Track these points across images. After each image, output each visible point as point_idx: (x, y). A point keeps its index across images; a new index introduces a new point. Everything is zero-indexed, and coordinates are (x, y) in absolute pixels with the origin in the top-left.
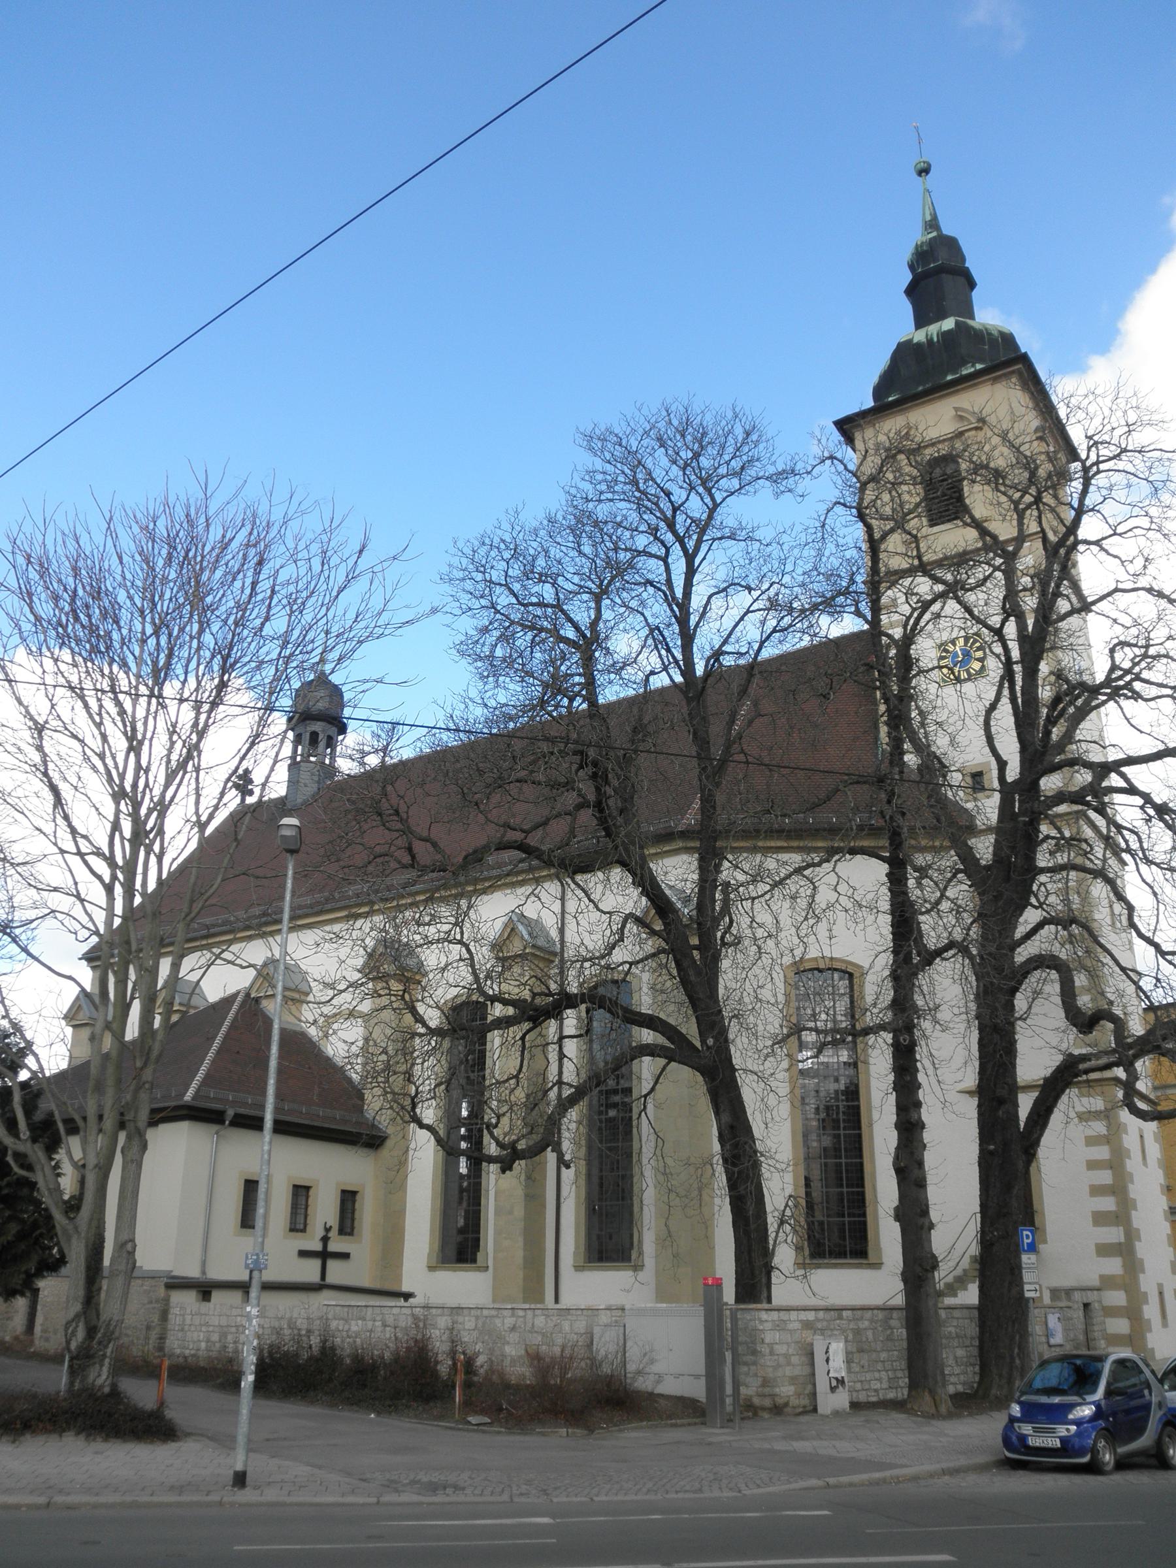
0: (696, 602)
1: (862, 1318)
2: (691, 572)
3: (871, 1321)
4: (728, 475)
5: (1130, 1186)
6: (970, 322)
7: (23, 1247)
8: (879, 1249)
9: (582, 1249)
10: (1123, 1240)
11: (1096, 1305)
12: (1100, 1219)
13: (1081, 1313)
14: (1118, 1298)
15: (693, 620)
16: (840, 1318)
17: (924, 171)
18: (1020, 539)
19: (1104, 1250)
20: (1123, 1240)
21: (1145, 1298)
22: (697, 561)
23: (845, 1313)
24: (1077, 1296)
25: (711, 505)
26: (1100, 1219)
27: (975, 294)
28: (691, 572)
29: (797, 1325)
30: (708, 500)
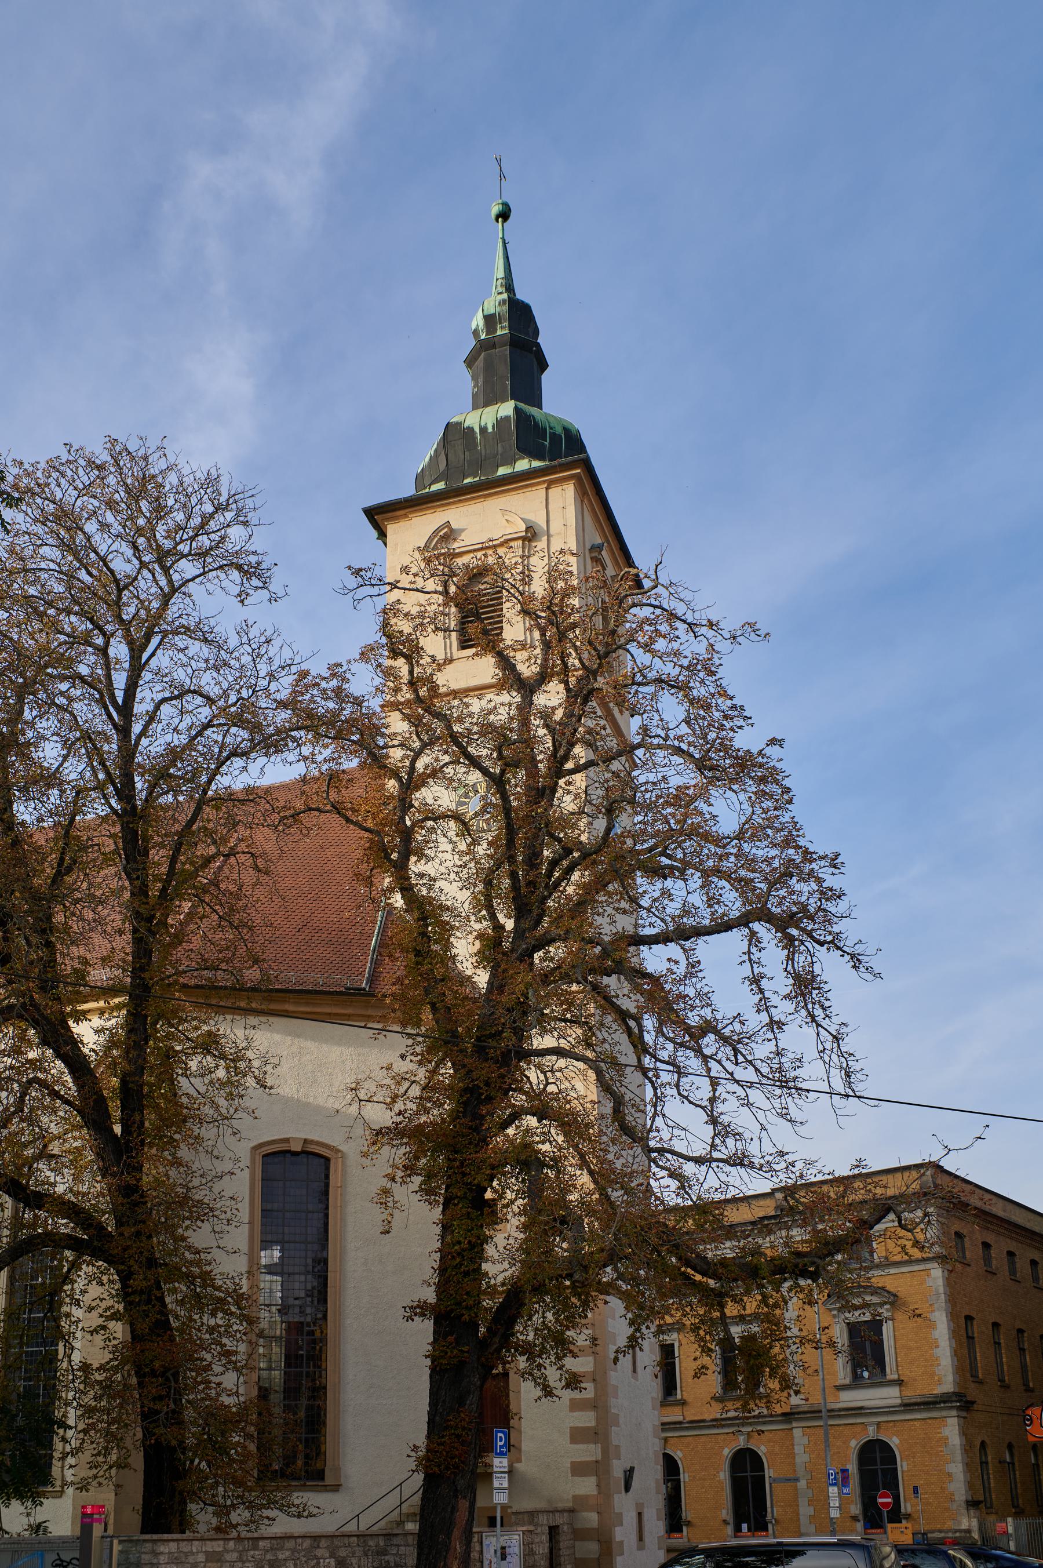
0: (140, 708)
1: (282, 1548)
2: (136, 669)
3: (293, 1551)
4: (190, 554)
5: (613, 1401)
6: (533, 411)
7: (674, 1259)
8: (337, 1470)
9: (330, 1416)
10: (599, 1458)
11: (565, 1528)
12: (578, 1435)
13: (545, 1538)
14: (591, 1519)
15: (137, 728)
16: (255, 1548)
17: (504, 215)
18: (543, 678)
19: (579, 1469)
20: (599, 1458)
21: (619, 1520)
22: (145, 656)
23: (261, 1544)
24: (543, 1519)
25: (166, 590)
26: (578, 1435)
27: (545, 377)
28: (136, 669)
29: (201, 1558)
30: (163, 582)
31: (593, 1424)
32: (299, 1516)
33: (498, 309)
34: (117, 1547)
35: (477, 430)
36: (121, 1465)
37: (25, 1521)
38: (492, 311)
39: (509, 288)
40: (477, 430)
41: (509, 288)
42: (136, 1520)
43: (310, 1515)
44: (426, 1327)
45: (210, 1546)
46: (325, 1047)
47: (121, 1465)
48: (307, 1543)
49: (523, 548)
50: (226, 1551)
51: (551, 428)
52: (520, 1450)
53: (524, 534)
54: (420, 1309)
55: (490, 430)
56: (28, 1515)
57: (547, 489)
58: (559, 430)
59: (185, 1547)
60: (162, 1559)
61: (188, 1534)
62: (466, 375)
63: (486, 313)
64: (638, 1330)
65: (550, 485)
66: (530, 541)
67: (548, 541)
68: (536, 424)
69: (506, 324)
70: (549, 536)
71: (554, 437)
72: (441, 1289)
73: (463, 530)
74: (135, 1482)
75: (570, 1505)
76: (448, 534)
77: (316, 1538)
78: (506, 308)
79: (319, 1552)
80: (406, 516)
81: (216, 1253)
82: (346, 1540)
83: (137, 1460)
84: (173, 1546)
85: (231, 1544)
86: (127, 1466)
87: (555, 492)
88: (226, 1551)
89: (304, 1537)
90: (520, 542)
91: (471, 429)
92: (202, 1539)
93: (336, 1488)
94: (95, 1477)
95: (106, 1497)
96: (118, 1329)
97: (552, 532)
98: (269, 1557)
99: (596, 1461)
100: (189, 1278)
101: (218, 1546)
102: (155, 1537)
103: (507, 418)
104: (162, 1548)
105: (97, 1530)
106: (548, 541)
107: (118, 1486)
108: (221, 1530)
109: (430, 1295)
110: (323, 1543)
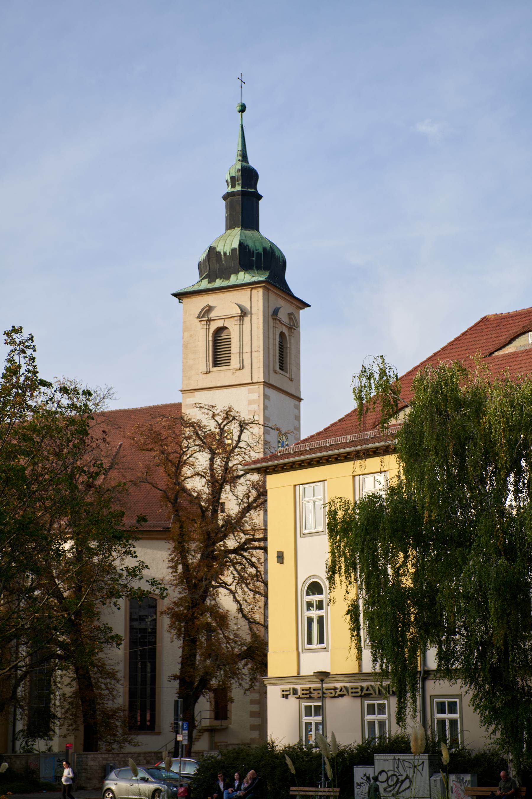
16: (118, 757)
23: (120, 755)
29: (101, 759)
31: (258, 710)
32: (135, 746)
33: (237, 174)
34: (76, 756)
35: (222, 253)
36: (76, 729)
37: (46, 747)
38: (234, 175)
39: (244, 157)
40: (222, 253)
41: (244, 157)
42: (82, 747)
43: (139, 746)
44: (177, 683)
45: (104, 756)
46: (155, 552)
47: (76, 729)
48: (136, 755)
49: (240, 320)
50: (109, 757)
51: (257, 250)
52: (231, 719)
53: (240, 315)
54: (175, 677)
55: (228, 254)
56: (47, 745)
57: (251, 290)
58: (261, 250)
59: (96, 756)
60: (89, 760)
61: (99, 752)
62: (224, 203)
63: (231, 175)
64: (253, 682)
65: (252, 289)
66: (243, 316)
67: (251, 317)
68: (249, 250)
69: (240, 182)
70: (251, 314)
71: (259, 255)
72: (182, 669)
73: (215, 307)
74: (81, 734)
75: (249, 742)
76: (209, 309)
77: (139, 754)
78: (240, 174)
79: (140, 758)
80: (190, 297)
81: (106, 659)
82: (150, 754)
83: (82, 728)
84: (92, 756)
85: (110, 755)
86: (78, 730)
87: (254, 291)
88: (109, 757)
89: (135, 753)
90: (239, 318)
91: (219, 253)
92: (101, 754)
93: (159, 734)
94: (68, 734)
95: (71, 739)
96: (74, 683)
97: (253, 312)
98: (123, 759)
99: (259, 725)
100: (98, 667)
101: (106, 756)
102: (87, 753)
103: (236, 249)
104: (89, 756)
105: (71, 751)
106: (251, 317)
107: (76, 736)
108: (108, 751)
109: (178, 673)
110: (142, 755)
